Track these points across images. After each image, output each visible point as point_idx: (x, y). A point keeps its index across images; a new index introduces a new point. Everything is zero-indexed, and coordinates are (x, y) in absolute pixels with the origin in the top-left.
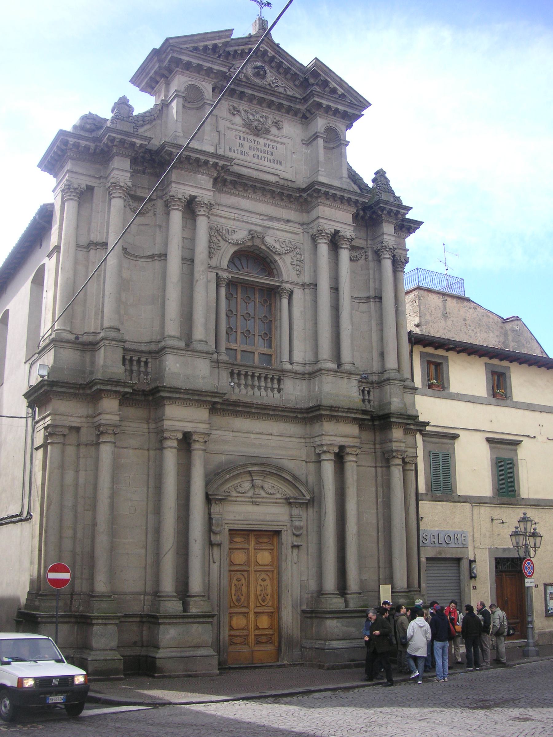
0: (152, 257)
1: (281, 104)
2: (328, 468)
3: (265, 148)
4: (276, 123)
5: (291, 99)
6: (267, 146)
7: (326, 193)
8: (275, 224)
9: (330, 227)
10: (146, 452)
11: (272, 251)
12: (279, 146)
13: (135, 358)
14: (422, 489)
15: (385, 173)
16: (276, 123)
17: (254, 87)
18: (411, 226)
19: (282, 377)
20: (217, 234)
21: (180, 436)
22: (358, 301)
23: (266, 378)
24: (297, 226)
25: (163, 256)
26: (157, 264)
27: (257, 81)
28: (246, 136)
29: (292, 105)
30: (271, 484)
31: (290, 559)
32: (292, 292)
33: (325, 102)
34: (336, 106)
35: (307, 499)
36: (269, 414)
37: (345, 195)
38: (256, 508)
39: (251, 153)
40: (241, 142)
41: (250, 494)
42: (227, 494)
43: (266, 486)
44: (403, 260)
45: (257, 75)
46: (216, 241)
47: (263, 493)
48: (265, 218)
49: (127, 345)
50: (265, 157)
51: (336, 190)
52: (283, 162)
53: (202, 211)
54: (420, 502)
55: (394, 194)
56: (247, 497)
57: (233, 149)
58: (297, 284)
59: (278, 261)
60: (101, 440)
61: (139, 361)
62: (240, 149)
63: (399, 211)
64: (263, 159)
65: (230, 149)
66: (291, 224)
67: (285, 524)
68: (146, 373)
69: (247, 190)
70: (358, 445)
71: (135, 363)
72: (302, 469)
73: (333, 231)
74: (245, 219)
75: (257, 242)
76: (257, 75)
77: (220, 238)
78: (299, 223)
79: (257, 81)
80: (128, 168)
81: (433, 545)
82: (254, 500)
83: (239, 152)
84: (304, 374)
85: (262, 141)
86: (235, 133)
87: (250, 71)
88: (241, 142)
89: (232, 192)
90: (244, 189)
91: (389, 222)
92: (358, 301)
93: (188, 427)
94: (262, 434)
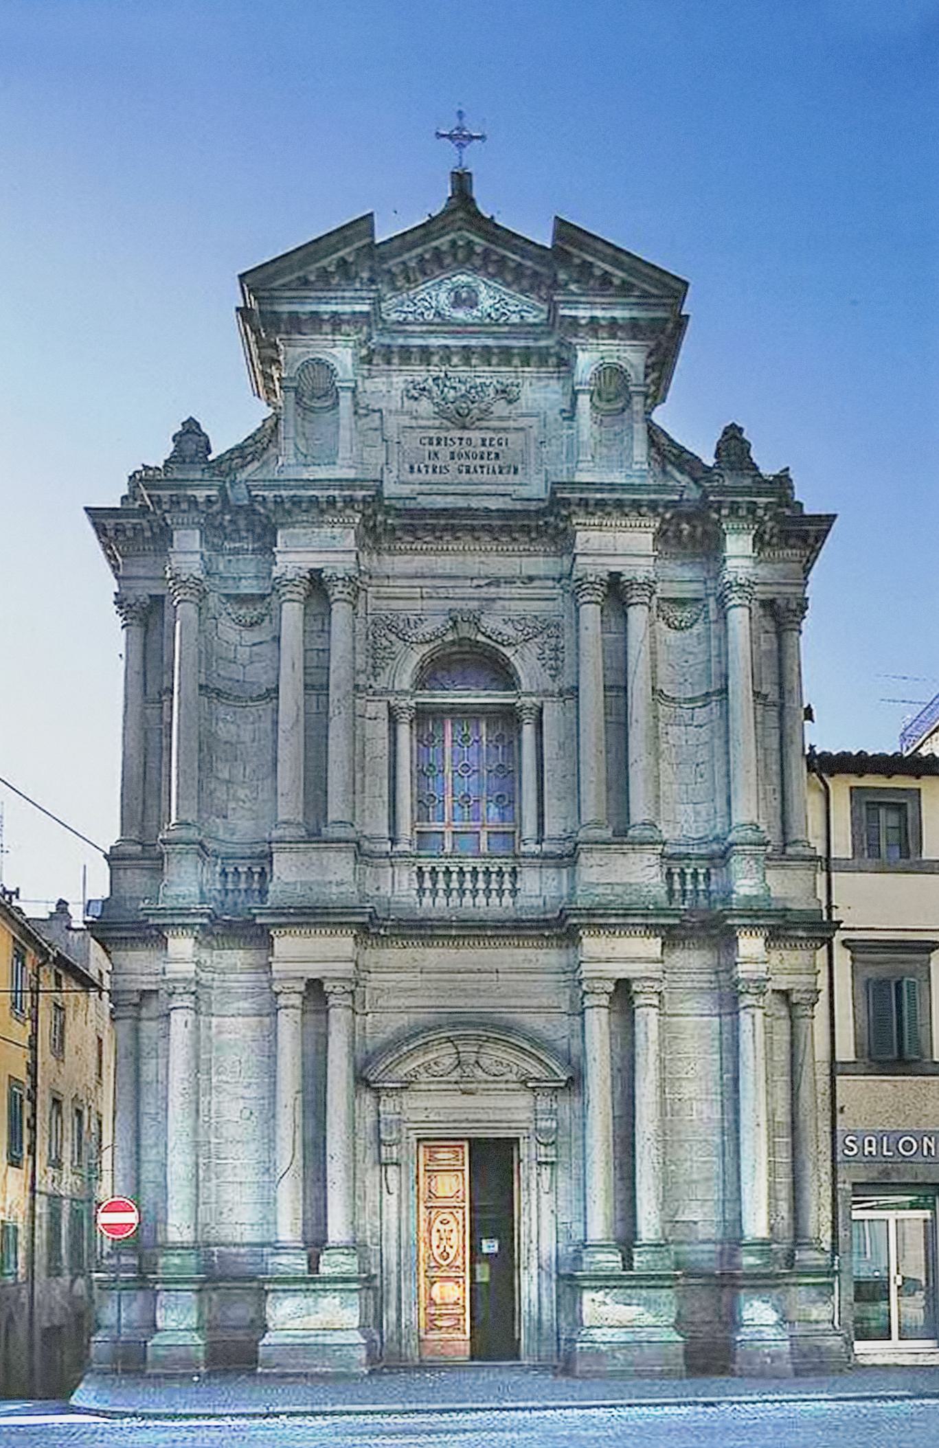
0: (260, 697)
1: (487, 348)
2: (598, 1023)
3: (483, 449)
4: (504, 392)
5: (523, 330)
6: (487, 443)
7: (584, 503)
8: (504, 591)
9: (600, 568)
10: (717, 1019)
11: (496, 641)
12: (512, 437)
13: (427, 869)
14: (845, 1052)
15: (741, 430)
16: (504, 392)
17: (461, 329)
18: (807, 531)
19: (518, 869)
20: (382, 635)
21: (301, 987)
22: (691, 706)
23: (487, 873)
24: (550, 583)
25: (273, 693)
26: (264, 707)
27: (460, 314)
28: (443, 434)
29: (531, 343)
30: (494, 1055)
31: (533, 1185)
32: (541, 711)
33: (583, 313)
34: (609, 314)
35: (561, 1081)
36: (451, 936)
37: (284, 493)
38: (469, 1101)
39: (453, 465)
40: (435, 448)
41: (455, 1076)
42: (410, 1079)
43: (485, 1061)
44: (793, 606)
45: (457, 303)
46: (386, 643)
47: (479, 1072)
48: (482, 583)
49: (668, 850)
50: (482, 467)
51: (600, 491)
52: (520, 467)
53: (635, 596)
54: (838, 1078)
55: (756, 468)
56: (449, 1082)
57: (416, 467)
58: (546, 693)
59: (512, 659)
60: (587, 1004)
61: (683, 874)
62: (431, 463)
63: (755, 503)
64: (479, 470)
65: (412, 468)
66: (536, 583)
67: (524, 1125)
68: (708, 893)
69: (441, 538)
70: (658, 975)
71: (468, 876)
72: (555, 1028)
73: (605, 576)
74: (443, 593)
75: (466, 631)
76: (457, 303)
77: (393, 638)
78: (554, 579)
79: (460, 314)
80: (749, 551)
81: (869, 1159)
82: (462, 1086)
83: (430, 470)
84: (561, 857)
85: (476, 436)
86: (418, 434)
87: (443, 299)
88: (435, 448)
89: (510, 548)
90: (436, 538)
91: (738, 531)
92: (691, 706)
93: (314, 971)
94: (479, 971)
